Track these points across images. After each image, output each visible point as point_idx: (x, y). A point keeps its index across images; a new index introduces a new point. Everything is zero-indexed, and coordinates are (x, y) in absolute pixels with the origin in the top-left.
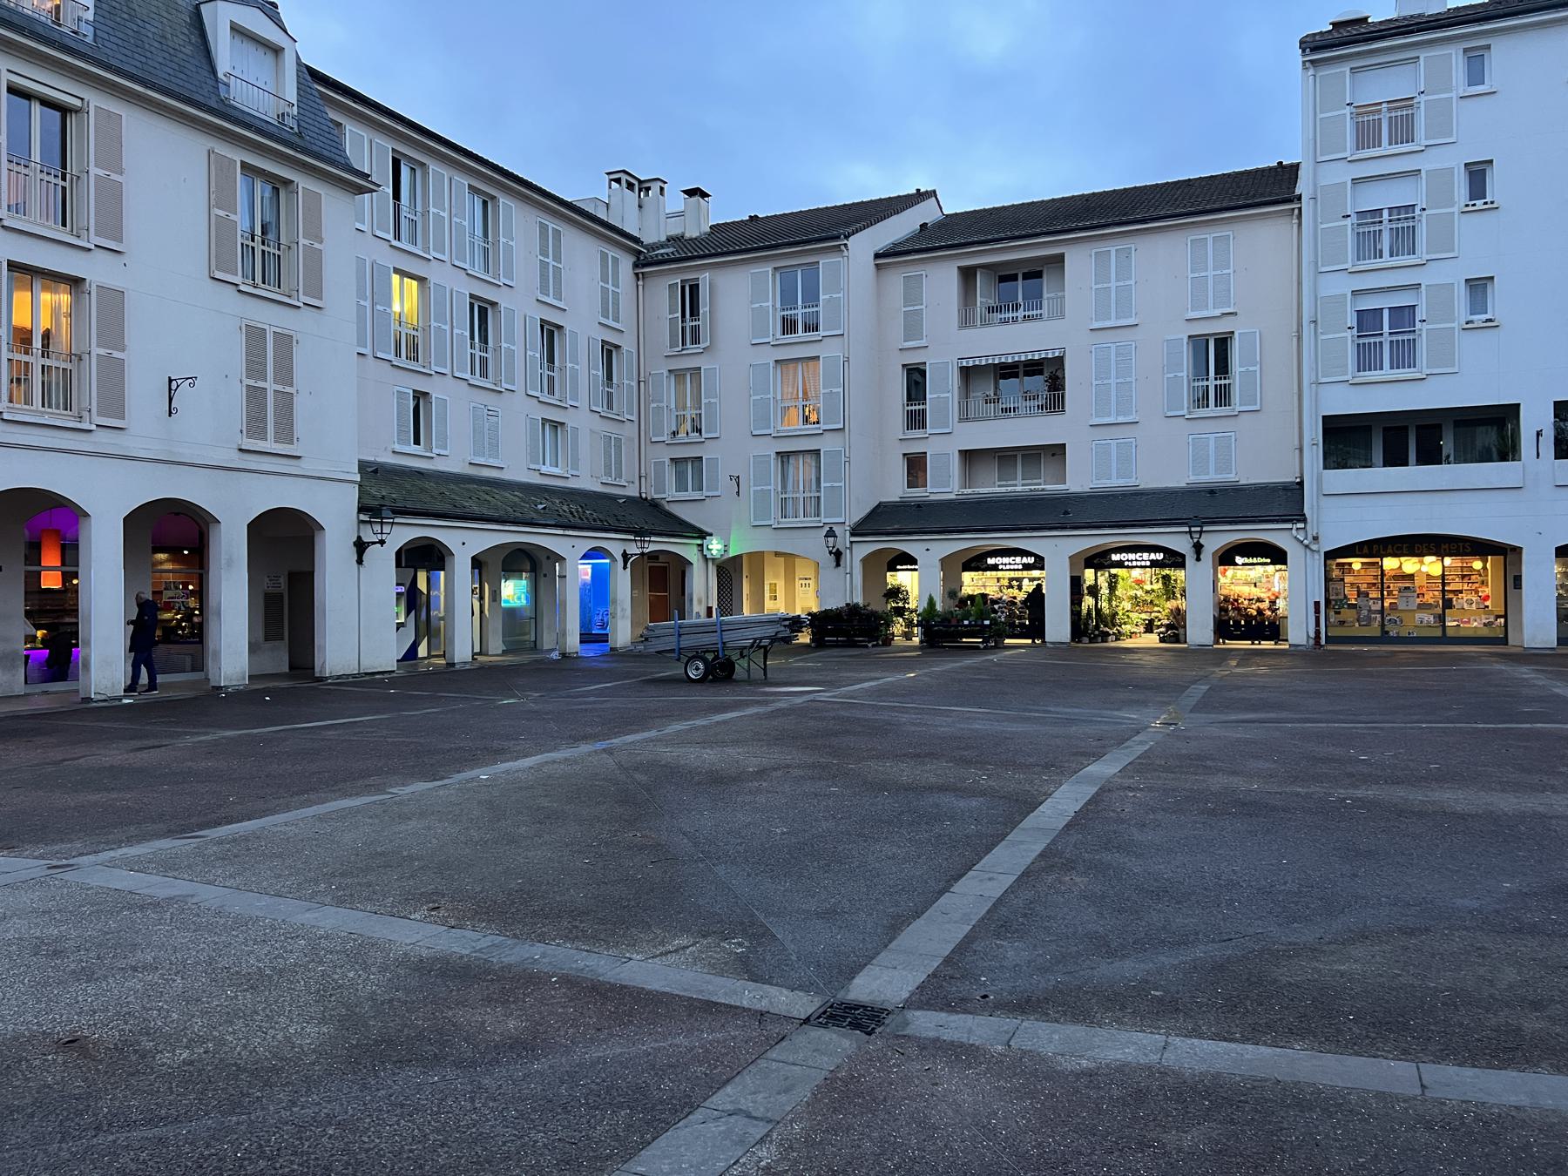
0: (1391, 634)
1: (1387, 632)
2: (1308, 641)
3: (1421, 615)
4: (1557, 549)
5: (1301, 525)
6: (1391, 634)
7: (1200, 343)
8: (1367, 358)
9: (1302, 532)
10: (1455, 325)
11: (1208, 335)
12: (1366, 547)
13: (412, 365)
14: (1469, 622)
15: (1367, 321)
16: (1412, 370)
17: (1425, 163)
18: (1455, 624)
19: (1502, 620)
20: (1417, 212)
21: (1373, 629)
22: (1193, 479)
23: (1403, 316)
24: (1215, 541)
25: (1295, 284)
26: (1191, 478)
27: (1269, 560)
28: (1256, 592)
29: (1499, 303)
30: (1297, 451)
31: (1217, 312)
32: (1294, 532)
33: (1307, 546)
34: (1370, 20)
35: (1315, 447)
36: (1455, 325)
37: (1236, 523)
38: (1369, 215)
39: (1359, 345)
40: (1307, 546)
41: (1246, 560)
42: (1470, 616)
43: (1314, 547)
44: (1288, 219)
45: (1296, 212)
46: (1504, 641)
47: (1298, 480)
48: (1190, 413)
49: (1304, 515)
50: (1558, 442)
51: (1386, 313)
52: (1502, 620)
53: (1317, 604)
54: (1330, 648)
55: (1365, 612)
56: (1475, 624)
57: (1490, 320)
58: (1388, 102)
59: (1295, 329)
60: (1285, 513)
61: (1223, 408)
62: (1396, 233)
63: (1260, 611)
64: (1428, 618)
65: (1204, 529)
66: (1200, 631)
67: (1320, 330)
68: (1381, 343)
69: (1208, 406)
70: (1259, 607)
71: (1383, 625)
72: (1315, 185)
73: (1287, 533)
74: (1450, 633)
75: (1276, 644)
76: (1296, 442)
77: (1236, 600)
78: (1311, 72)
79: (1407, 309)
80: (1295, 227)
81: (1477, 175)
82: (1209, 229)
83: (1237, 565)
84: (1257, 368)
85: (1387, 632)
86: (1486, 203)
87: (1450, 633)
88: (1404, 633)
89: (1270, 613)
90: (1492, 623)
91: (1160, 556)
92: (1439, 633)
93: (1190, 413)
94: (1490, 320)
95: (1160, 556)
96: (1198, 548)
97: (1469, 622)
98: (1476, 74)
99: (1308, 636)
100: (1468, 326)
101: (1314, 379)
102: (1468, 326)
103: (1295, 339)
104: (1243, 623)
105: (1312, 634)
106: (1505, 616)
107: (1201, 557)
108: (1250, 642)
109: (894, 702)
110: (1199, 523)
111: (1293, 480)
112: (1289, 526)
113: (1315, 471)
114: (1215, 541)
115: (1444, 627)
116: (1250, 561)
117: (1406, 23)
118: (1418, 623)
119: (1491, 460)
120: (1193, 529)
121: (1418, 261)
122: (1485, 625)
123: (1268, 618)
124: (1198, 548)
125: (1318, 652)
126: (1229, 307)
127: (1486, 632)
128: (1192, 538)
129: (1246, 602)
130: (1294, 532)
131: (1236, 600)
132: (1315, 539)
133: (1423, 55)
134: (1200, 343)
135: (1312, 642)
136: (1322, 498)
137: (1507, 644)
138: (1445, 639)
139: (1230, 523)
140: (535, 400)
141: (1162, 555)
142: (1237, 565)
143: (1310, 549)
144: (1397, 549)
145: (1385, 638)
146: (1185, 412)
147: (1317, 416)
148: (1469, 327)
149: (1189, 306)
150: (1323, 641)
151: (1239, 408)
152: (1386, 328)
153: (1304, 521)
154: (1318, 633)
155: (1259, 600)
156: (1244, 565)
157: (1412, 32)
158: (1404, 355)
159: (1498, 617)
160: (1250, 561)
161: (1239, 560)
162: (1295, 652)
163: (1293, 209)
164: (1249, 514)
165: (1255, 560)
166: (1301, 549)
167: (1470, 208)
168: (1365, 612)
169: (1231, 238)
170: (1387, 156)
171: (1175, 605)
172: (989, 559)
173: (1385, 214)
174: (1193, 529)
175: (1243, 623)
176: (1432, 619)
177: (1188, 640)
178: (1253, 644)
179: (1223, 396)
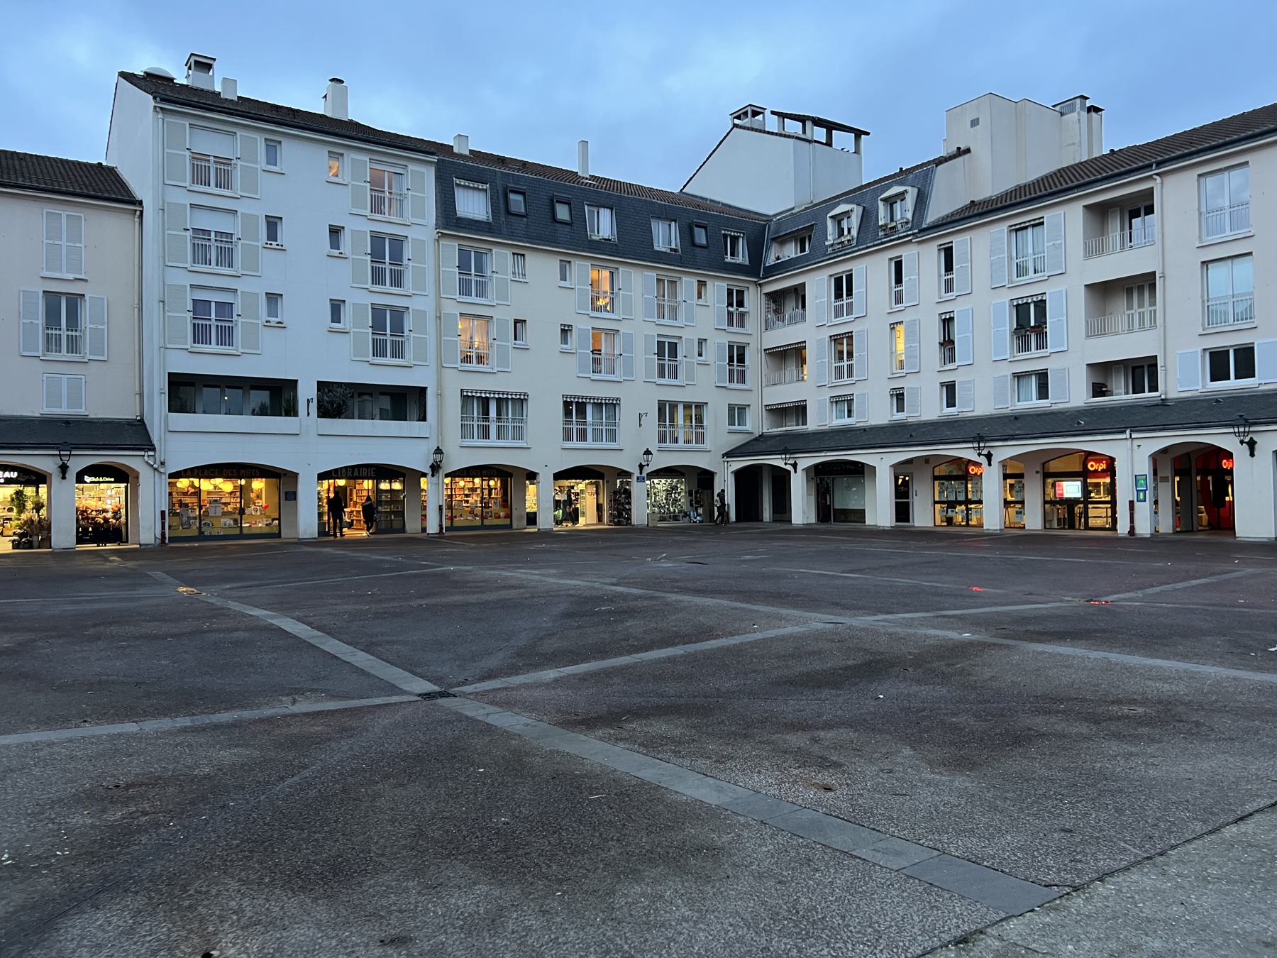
0: (206, 533)
1: (203, 532)
2: (155, 541)
3: (225, 520)
4: (319, 475)
5: (150, 453)
6: (206, 533)
7: (52, 299)
8: (200, 334)
9: (152, 458)
10: (259, 322)
11: (62, 293)
12: (356, 469)
13: (673, 382)
14: (255, 523)
15: (200, 307)
16: (231, 347)
17: (242, 207)
18: (248, 525)
19: (277, 522)
20: (234, 239)
21: (194, 531)
22: (46, 410)
23: (226, 308)
24: (78, 463)
25: (137, 267)
26: (45, 409)
27: (113, 480)
28: (101, 506)
29: (287, 310)
30: (138, 396)
31: (71, 276)
32: (146, 458)
33: (156, 469)
34: (175, 81)
35: (163, 395)
36: (259, 322)
37: (98, 449)
38: (200, 232)
39: (194, 324)
40: (156, 469)
41: (94, 479)
42: (256, 522)
43: (162, 470)
44: (131, 217)
45: (138, 213)
46: (279, 535)
47: (139, 418)
48: (44, 355)
49: (153, 445)
50: (319, 407)
51: (213, 305)
52: (277, 522)
53: (163, 513)
54: (172, 545)
55: (185, 519)
56: (260, 525)
57: (280, 323)
58: (215, 157)
59: (136, 302)
60: (137, 443)
61: (74, 354)
62: (220, 250)
63: (106, 520)
64: (230, 522)
65: (72, 453)
66: (64, 536)
67: (167, 309)
68: (210, 325)
69: (60, 352)
70: (105, 517)
71: (200, 527)
72: (163, 201)
73: (141, 458)
74: (245, 531)
75: (119, 545)
76: (137, 390)
77: (86, 511)
78: (160, 116)
79: (227, 305)
80: (137, 224)
81: (273, 224)
82: (66, 208)
83: (86, 483)
84: (105, 327)
85: (203, 532)
86: (278, 245)
87: (245, 531)
88: (215, 533)
89: (114, 521)
90: (270, 524)
91: (14, 475)
92: (237, 531)
93: (44, 355)
94: (280, 323)
95: (14, 475)
96: (64, 469)
97: (255, 523)
98: (272, 160)
99: (155, 537)
100: (268, 324)
101: (162, 344)
102: (268, 324)
103: (136, 310)
104: (90, 529)
105: (159, 535)
106: (279, 519)
107: (67, 476)
108: (1199, 489)
109: (295, 582)
110: (67, 448)
111: (134, 417)
112: (142, 453)
113: (163, 414)
114: (78, 463)
115: (241, 527)
116: (97, 479)
117: (230, 106)
118: (223, 526)
119: (281, 415)
120: (62, 453)
121: (234, 273)
122: (267, 525)
123: (114, 525)
124: (64, 469)
125: (166, 546)
126: (81, 274)
127: (267, 530)
128: (61, 460)
129: (94, 513)
130: (146, 458)
131: (86, 511)
132: (163, 463)
133: (240, 133)
134: (52, 299)
135: (158, 541)
136: (168, 434)
137: (280, 537)
138: (242, 536)
139: (93, 449)
140: (366, 364)
141: (16, 474)
142: (86, 483)
143: (158, 471)
144: (212, 472)
145: (201, 537)
146: (40, 354)
147: (164, 371)
148: (267, 325)
149: (44, 266)
150: (167, 541)
151: (89, 357)
152: (213, 316)
153: (154, 450)
154: (163, 534)
155: (105, 511)
156: (91, 483)
157: (232, 114)
158: (226, 336)
159: (273, 520)
160: (97, 479)
161: (87, 479)
162: (144, 551)
163: (136, 210)
164: (107, 443)
165: (101, 479)
166: (151, 471)
167: (269, 246)
168: (185, 519)
169: (83, 219)
170: (212, 195)
171: (29, 516)
172: (86, 477)
173: (213, 234)
174: (62, 453)
175: (90, 529)
176: (232, 522)
177: (52, 545)
178: (99, 546)
179: (74, 345)
